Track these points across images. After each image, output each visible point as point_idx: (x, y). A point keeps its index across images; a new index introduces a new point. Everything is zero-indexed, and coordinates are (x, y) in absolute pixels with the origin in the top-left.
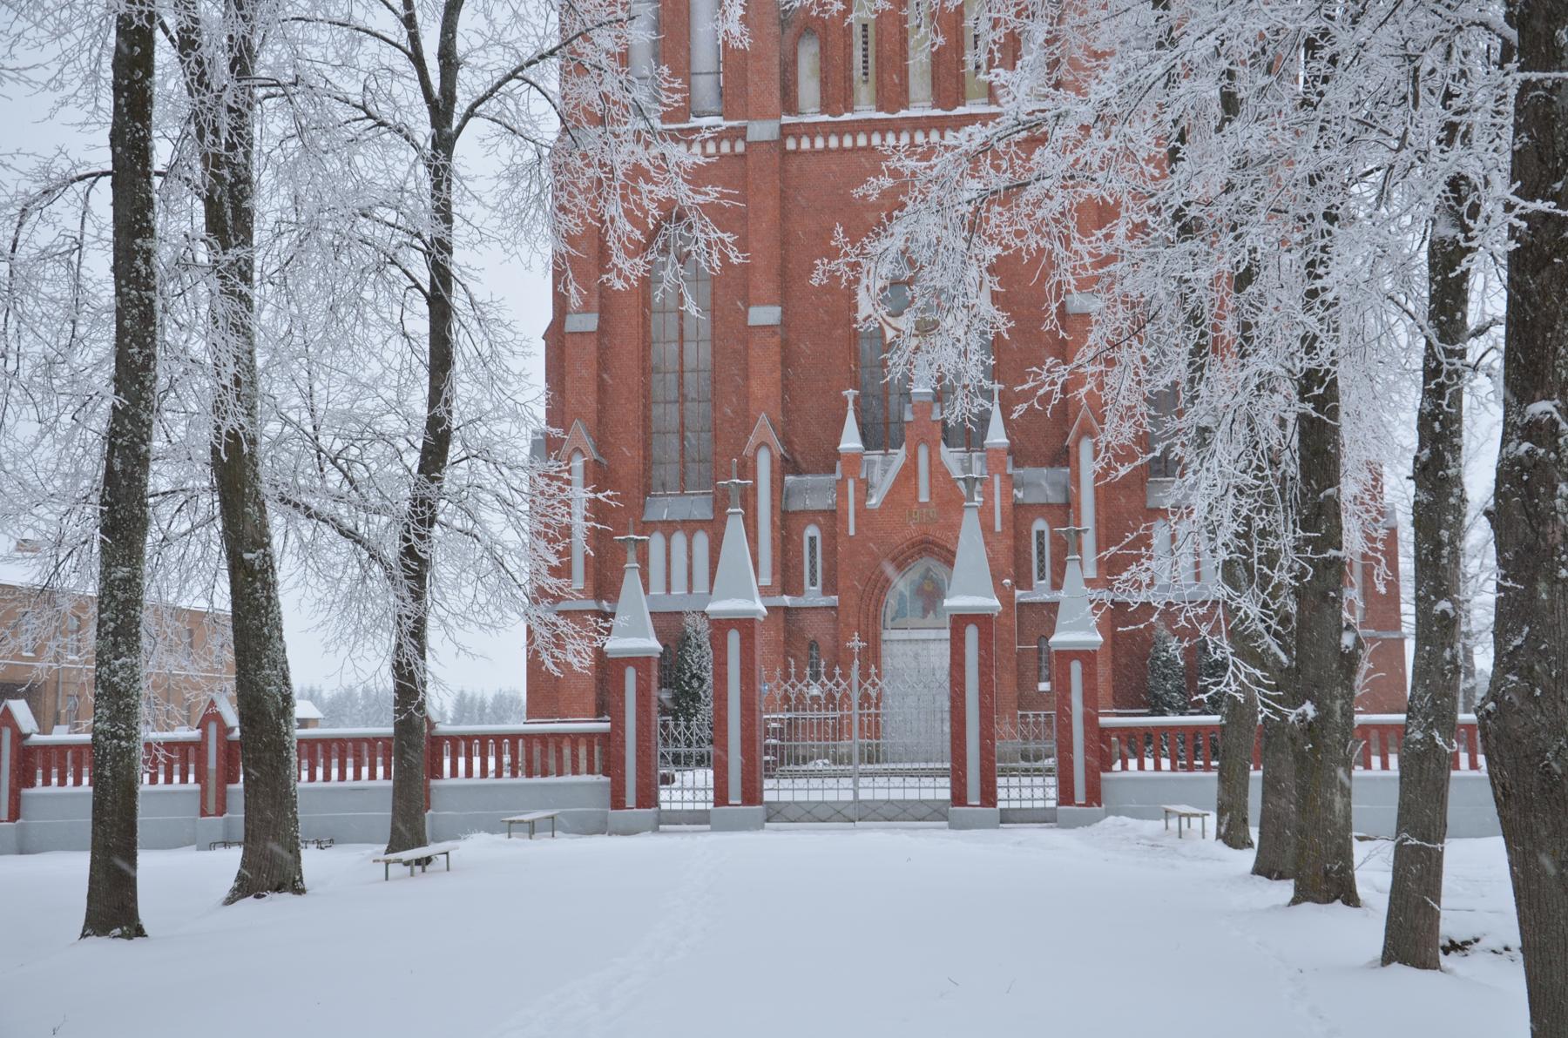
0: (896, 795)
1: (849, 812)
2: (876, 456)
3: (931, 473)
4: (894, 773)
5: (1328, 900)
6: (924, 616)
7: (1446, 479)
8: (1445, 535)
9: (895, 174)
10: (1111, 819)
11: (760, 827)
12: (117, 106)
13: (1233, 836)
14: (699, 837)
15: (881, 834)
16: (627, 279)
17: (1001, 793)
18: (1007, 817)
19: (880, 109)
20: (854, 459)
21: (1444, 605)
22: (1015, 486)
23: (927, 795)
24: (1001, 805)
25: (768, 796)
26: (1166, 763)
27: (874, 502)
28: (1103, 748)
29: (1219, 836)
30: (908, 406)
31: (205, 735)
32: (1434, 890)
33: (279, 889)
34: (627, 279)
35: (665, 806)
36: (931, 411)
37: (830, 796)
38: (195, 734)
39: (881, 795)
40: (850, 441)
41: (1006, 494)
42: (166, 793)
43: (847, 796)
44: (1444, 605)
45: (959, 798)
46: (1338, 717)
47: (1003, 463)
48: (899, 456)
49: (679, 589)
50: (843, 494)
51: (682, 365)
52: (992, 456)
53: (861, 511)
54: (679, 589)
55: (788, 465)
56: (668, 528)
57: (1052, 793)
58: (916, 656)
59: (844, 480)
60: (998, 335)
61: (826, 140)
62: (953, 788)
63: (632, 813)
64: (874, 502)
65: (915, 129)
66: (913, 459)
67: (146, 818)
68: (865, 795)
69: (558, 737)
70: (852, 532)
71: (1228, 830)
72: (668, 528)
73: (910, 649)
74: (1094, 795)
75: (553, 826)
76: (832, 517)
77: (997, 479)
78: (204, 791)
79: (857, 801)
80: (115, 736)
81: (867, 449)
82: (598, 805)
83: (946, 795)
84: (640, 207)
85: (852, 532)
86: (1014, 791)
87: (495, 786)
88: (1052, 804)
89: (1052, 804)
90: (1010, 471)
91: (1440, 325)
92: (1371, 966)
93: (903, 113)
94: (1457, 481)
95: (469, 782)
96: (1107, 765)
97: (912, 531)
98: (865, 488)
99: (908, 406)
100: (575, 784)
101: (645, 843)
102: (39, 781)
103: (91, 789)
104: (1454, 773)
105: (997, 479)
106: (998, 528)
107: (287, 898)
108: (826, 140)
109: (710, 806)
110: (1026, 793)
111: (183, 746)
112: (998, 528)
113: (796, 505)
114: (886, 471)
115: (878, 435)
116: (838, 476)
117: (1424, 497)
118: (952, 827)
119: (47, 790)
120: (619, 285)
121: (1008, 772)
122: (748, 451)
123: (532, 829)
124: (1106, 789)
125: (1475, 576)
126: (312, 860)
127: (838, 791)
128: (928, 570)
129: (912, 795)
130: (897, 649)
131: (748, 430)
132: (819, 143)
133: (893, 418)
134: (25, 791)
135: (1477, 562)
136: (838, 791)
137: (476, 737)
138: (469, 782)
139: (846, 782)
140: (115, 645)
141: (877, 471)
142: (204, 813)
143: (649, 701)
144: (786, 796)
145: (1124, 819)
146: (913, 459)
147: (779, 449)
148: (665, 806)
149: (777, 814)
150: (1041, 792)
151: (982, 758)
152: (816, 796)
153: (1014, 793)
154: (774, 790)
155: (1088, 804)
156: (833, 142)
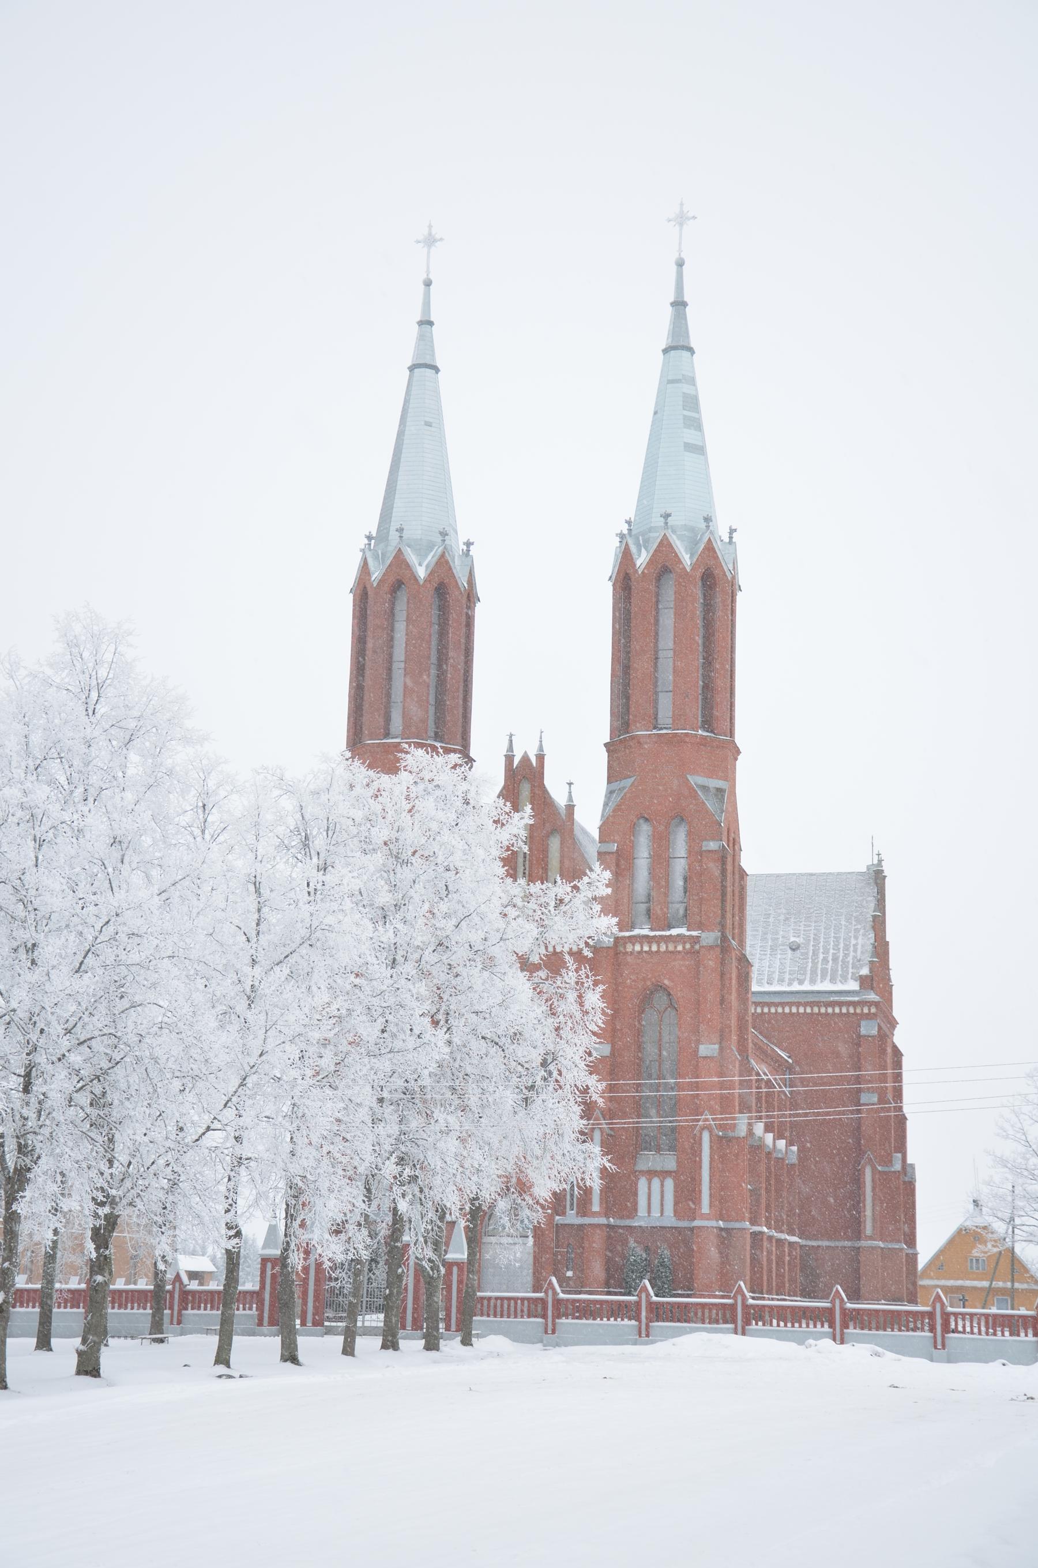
12: (742, 942)
26: (1007, 1333)
31: (174, 1288)
38: (928, 1309)
42: (607, 1325)
49: (656, 1213)
54: (656, 1213)
56: (651, 1174)
61: (783, 1009)
62: (385, 1321)
65: (849, 1006)
69: (899, 1312)
72: (651, 1174)
78: (935, 1337)
87: (761, 1330)
96: (749, 1323)
100: (488, 1321)
102: (190, 1308)
108: (783, 1009)
111: (923, 1314)
119: (205, 1312)
126: (54, 1341)
132: (852, 1010)
134: (184, 1312)
137: (960, 1314)
142: (546, 1332)
156: (816, 1010)
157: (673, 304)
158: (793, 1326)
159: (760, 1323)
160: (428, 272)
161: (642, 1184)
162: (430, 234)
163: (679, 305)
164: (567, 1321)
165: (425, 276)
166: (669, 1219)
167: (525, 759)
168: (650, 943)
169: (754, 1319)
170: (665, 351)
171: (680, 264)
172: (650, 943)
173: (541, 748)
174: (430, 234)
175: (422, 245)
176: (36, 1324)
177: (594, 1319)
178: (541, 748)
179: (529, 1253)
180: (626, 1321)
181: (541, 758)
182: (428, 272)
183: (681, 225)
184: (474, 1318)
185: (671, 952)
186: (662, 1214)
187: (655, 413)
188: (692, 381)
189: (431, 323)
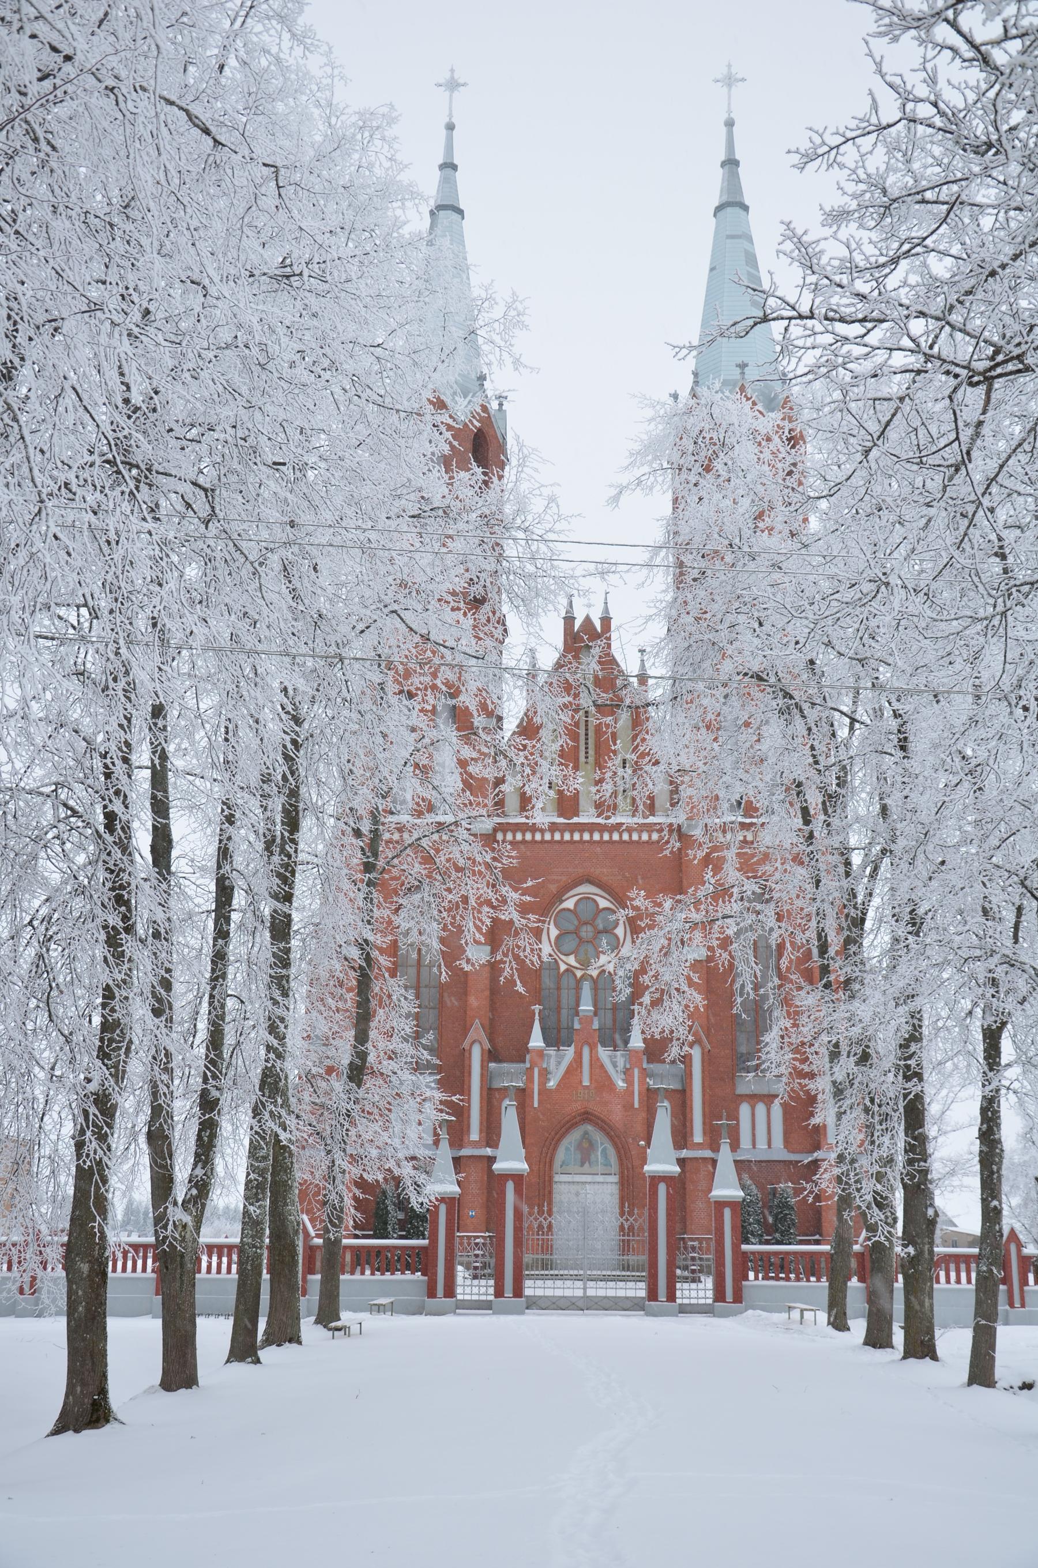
0: (611, 1293)
1: (580, 1304)
2: (551, 1051)
3: (591, 1065)
4: (562, 1277)
5: (922, 1357)
6: (582, 1165)
7: (994, 1140)
8: (995, 1168)
9: (636, 908)
10: (750, 1312)
11: (522, 1313)
13: (839, 1323)
14: (487, 1318)
15: (619, 1318)
16: (473, 965)
17: (678, 1294)
18: (684, 1310)
19: (559, 816)
20: (540, 1053)
21: (995, 1203)
22: (647, 1076)
23: (631, 1293)
24: (679, 1301)
25: (528, 1292)
27: (552, 1084)
28: (743, 1264)
29: (829, 1323)
30: (576, 1019)
32: (992, 1347)
33: (290, 1341)
34: (473, 965)
35: (459, 1297)
36: (592, 1022)
37: (568, 1293)
39: (601, 1293)
40: (536, 1041)
41: (642, 1082)
43: (579, 1293)
44: (995, 1203)
45: (653, 1295)
46: (926, 1255)
47: (641, 1061)
48: (570, 1052)
49: (762, 1145)
50: (530, 1079)
51: (418, 981)
52: (633, 1054)
53: (543, 1091)
54: (762, 1145)
55: (492, 1055)
56: (753, 1099)
57: (491, 1290)
58: (577, 1194)
59: (530, 1070)
60: (697, 1008)
63: (441, 1301)
64: (552, 1084)
66: (579, 1055)
67: (113, 1294)
68: (591, 1293)
70: (536, 1105)
71: (836, 1318)
72: (753, 1099)
73: (573, 1188)
74: (738, 1298)
75: (392, 1309)
76: (522, 1095)
77: (636, 1071)
79: (585, 1297)
80: (254, 1246)
81: (548, 1045)
82: (419, 1296)
83: (643, 1294)
84: (480, 920)
85: (536, 1105)
86: (689, 1293)
88: (710, 1301)
89: (710, 1301)
90: (645, 1066)
91: (989, 1064)
92: (962, 1386)
93: (575, 820)
94: (999, 1142)
95: (134, 1275)
97: (577, 1107)
98: (545, 1074)
99: (576, 1019)
101: (448, 1320)
103: (64, 1274)
104: (197, 1276)
105: (636, 1071)
106: (636, 1105)
107: (294, 1345)
109: (492, 1298)
110: (694, 1294)
112: (636, 1105)
113: (498, 1084)
114: (559, 1063)
115: (554, 1038)
116: (528, 1065)
117: (985, 1149)
118: (648, 1314)
120: (467, 968)
121: (530, 1277)
122: (466, 1044)
123: (380, 1309)
124: (746, 1293)
125: (935, 1138)
127: (572, 1290)
128: (586, 1133)
129: (621, 1293)
130: (563, 1188)
131: (465, 1031)
133: (564, 1024)
135: (936, 1128)
136: (572, 1290)
138: (134, 1275)
139: (579, 1284)
140: (257, 1194)
141: (553, 1062)
143: (717, 1251)
144: (539, 1292)
145: (759, 1312)
146: (579, 1055)
147: (487, 1045)
148: (459, 1297)
149: (534, 1304)
150: (703, 1291)
151: (515, 1263)
152: (559, 1293)
153: (483, 1290)
154: (532, 1288)
155: (734, 1302)
157: (723, 164)
158: (808, 1280)
159: (813, 1279)
160: (450, 115)
161: (744, 1110)
162: (452, 78)
163: (731, 163)
164: (403, 1277)
165: (447, 120)
166: (779, 1151)
167: (588, 620)
168: (601, 832)
169: (753, 1269)
170: (719, 209)
171: (730, 124)
172: (601, 832)
173: (606, 610)
174: (452, 78)
175: (443, 88)
176: (231, 1297)
177: (383, 1274)
178: (606, 610)
179: (612, 1195)
180: (408, 1276)
181: (606, 621)
182: (450, 115)
183: (730, 86)
184: (342, 1277)
185: (637, 842)
186: (769, 1146)
187: (712, 269)
188: (750, 240)
189: (454, 167)
